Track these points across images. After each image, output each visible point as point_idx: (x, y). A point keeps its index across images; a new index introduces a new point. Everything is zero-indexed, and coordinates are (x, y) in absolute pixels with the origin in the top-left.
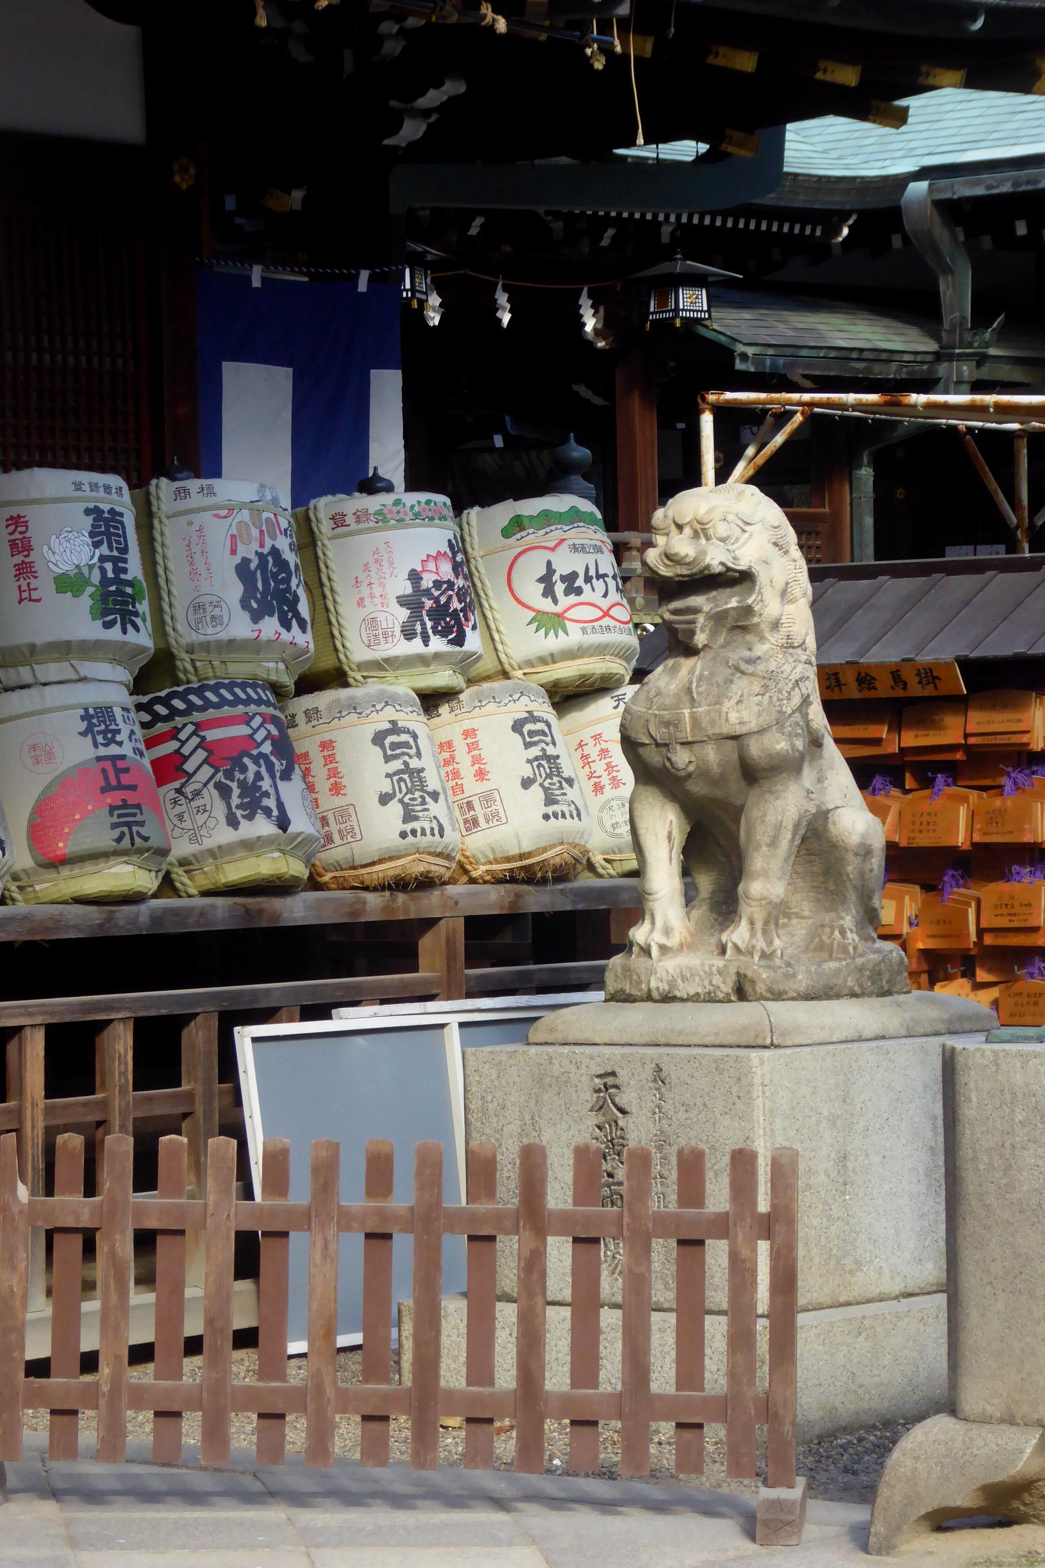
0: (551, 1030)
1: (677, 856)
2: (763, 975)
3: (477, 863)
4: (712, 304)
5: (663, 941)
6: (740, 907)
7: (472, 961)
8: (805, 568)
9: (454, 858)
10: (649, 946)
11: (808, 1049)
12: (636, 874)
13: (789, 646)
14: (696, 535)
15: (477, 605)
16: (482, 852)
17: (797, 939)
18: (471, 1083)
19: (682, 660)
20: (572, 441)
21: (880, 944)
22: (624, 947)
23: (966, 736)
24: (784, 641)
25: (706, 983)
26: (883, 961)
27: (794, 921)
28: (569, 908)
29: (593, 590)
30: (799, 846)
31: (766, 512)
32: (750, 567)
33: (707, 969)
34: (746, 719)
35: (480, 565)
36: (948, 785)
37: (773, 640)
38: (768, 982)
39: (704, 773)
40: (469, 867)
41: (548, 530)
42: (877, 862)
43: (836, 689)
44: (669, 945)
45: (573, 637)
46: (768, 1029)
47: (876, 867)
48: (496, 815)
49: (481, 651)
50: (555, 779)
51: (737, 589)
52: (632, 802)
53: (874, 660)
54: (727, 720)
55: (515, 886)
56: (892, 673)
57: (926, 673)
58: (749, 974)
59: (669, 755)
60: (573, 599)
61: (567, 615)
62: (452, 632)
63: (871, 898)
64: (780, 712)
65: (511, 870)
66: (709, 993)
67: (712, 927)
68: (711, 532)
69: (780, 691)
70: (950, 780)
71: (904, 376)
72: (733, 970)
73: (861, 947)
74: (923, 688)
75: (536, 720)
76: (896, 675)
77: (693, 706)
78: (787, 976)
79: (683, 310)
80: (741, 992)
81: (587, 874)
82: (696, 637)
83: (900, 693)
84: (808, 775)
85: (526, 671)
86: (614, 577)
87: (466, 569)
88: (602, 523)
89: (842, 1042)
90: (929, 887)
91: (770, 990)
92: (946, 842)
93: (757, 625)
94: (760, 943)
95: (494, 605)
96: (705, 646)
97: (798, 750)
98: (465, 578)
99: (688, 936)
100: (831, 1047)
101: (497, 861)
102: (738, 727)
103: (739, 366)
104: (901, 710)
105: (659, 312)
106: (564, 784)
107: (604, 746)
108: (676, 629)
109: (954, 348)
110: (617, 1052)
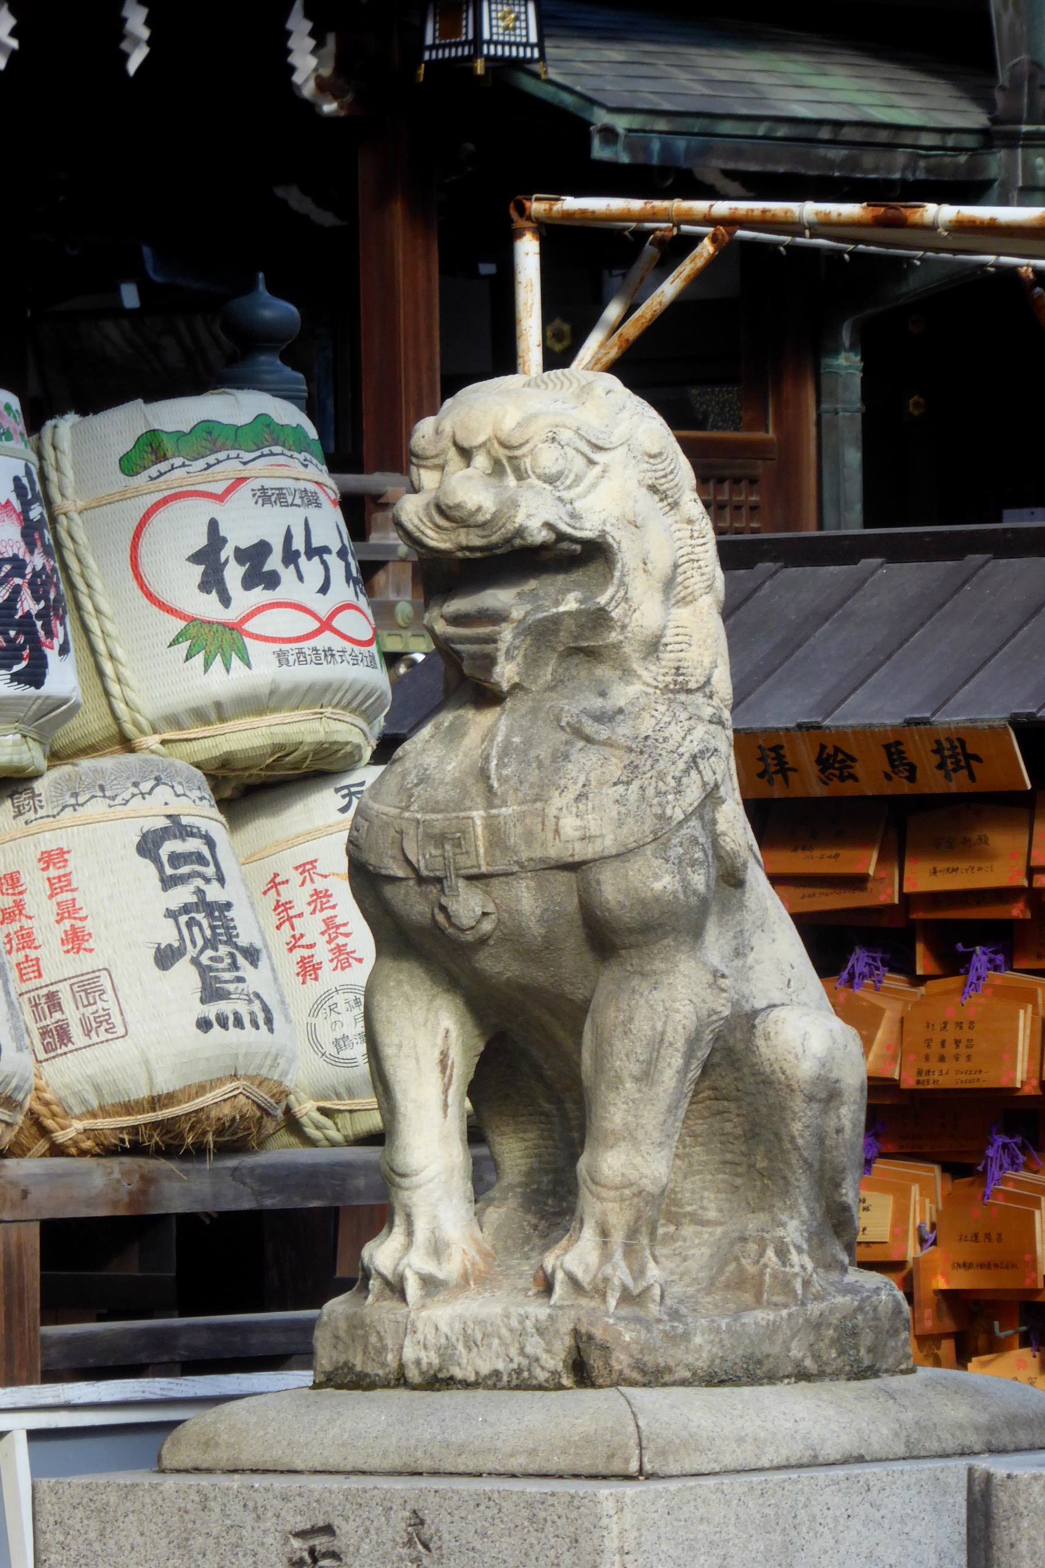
0: (207, 1444)
1: (460, 1104)
2: (624, 1337)
3: (67, 1114)
4: (546, 31)
5: (429, 1267)
6: (581, 1202)
7: (53, 1309)
8: (711, 537)
9: (20, 1105)
10: (402, 1278)
11: (711, 1482)
12: (377, 1139)
13: (679, 688)
14: (497, 469)
15: (70, 605)
16: (75, 1094)
17: (692, 1265)
18: (47, 1547)
19: (469, 714)
20: (262, 287)
21: (855, 1276)
22: (357, 1280)
23: (1031, 872)
24: (669, 679)
25: (513, 1352)
26: (860, 1309)
27: (688, 1230)
28: (247, 1204)
29: (301, 578)
30: (698, 1082)
31: (640, 426)
32: (603, 533)
33: (514, 1323)
34: (594, 830)
35: (78, 529)
36: (996, 968)
37: (647, 676)
38: (635, 1349)
39: (512, 937)
40: (49, 1123)
41: (211, 459)
42: (850, 1115)
43: (778, 778)
44: (441, 1275)
45: (262, 669)
46: (633, 1442)
47: (847, 1124)
48: (104, 1020)
49: (76, 696)
50: (223, 950)
51: (576, 576)
52: (370, 992)
53: (851, 722)
54: (557, 831)
55: (141, 1161)
56: (887, 747)
57: (953, 748)
58: (598, 1333)
59: (444, 901)
60: (259, 595)
61: (248, 626)
62: (20, 659)
63: (838, 1186)
64: (661, 817)
65: (134, 1130)
66: (519, 1371)
67: (527, 1239)
68: (527, 463)
69: (661, 776)
70: (1000, 958)
71: (921, 175)
72: (565, 1326)
73: (818, 1281)
74: (947, 777)
75: (184, 832)
76: (894, 751)
77: (490, 805)
78: (672, 1338)
79: (490, 42)
80: (582, 1371)
81: (285, 1138)
82: (498, 669)
83: (905, 788)
84: (716, 944)
85: (167, 736)
86: (342, 554)
87: (48, 535)
88: (318, 448)
89: (778, 1468)
90: (955, 1169)
91: (639, 1366)
92: (990, 1079)
93: (617, 646)
94: (620, 1273)
95: (104, 606)
96: (516, 687)
97: (695, 892)
98: (47, 552)
99: (478, 1258)
100: (756, 1478)
101: (105, 1111)
102: (578, 846)
103: (599, 151)
104: (904, 820)
105: (443, 47)
106: (241, 960)
107: (320, 884)
108: (457, 653)
109: (1020, 122)
110: (335, 1486)
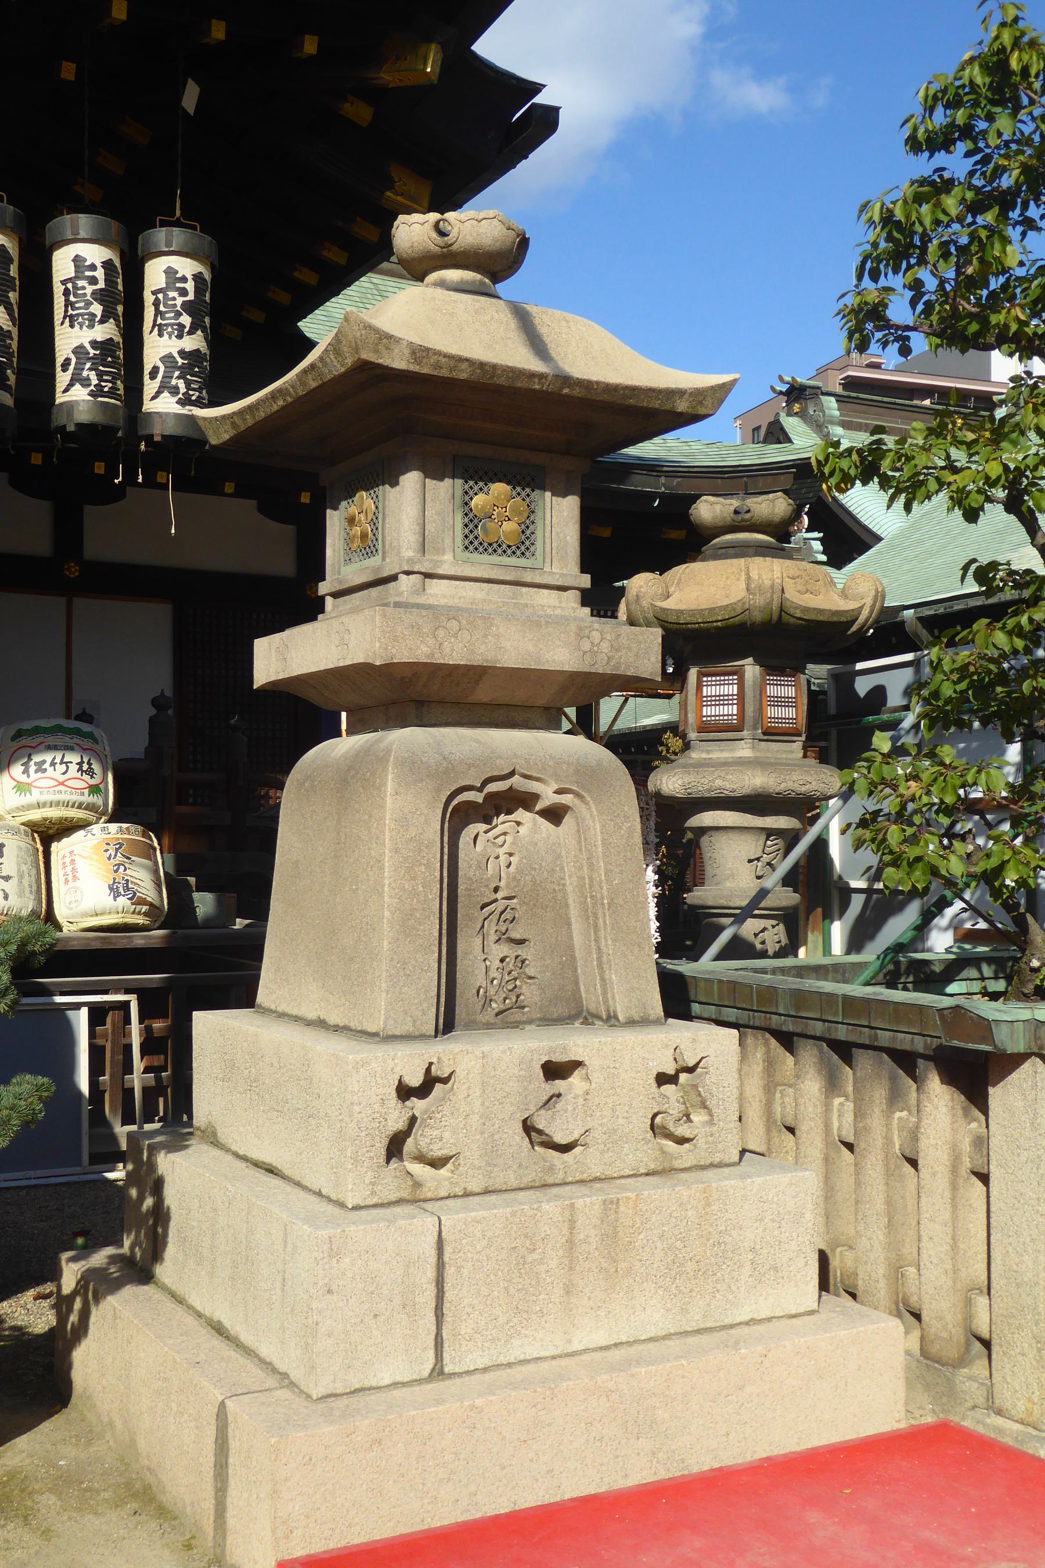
60: (40, 775)
